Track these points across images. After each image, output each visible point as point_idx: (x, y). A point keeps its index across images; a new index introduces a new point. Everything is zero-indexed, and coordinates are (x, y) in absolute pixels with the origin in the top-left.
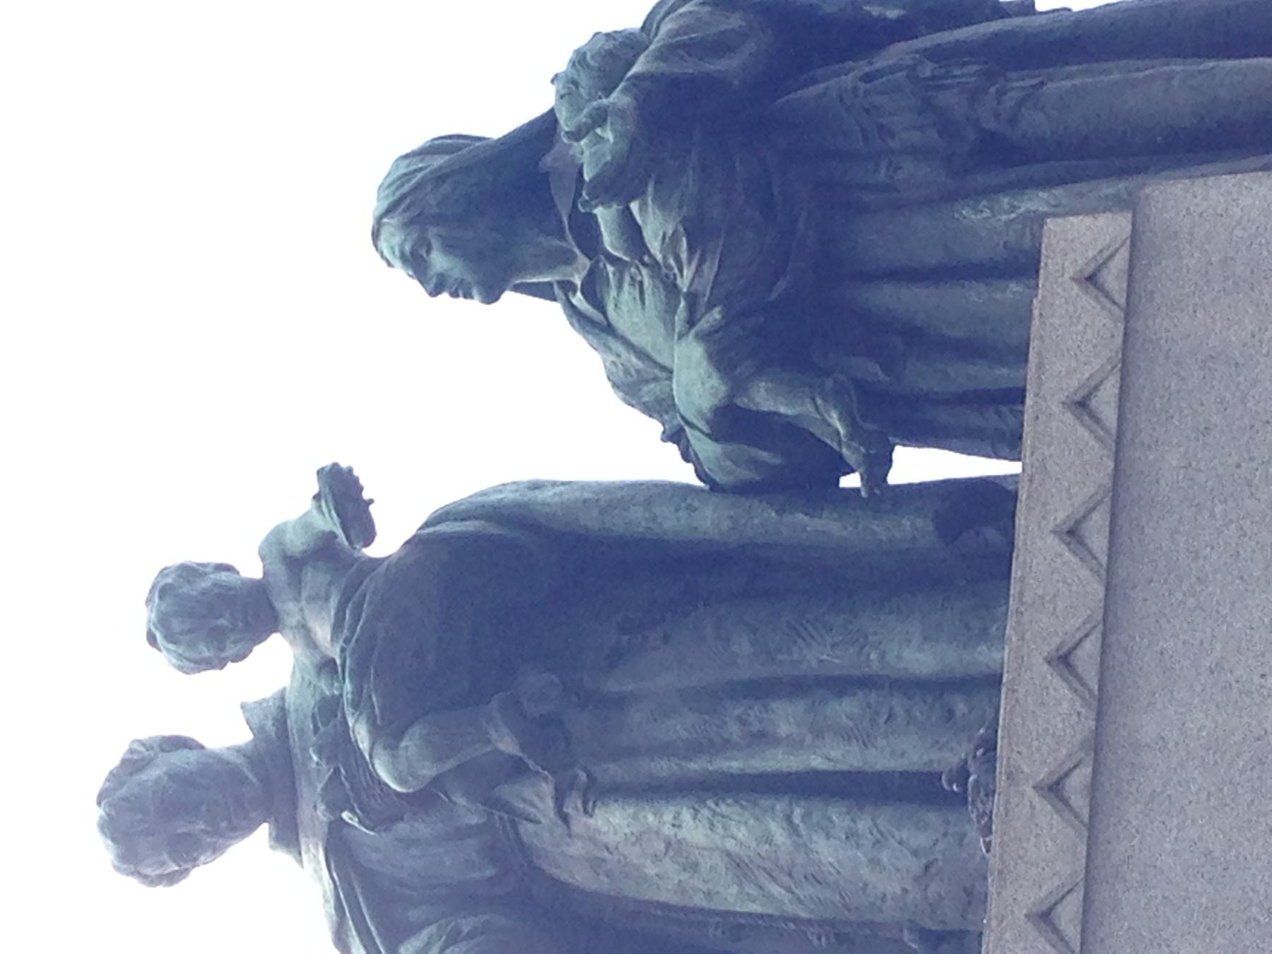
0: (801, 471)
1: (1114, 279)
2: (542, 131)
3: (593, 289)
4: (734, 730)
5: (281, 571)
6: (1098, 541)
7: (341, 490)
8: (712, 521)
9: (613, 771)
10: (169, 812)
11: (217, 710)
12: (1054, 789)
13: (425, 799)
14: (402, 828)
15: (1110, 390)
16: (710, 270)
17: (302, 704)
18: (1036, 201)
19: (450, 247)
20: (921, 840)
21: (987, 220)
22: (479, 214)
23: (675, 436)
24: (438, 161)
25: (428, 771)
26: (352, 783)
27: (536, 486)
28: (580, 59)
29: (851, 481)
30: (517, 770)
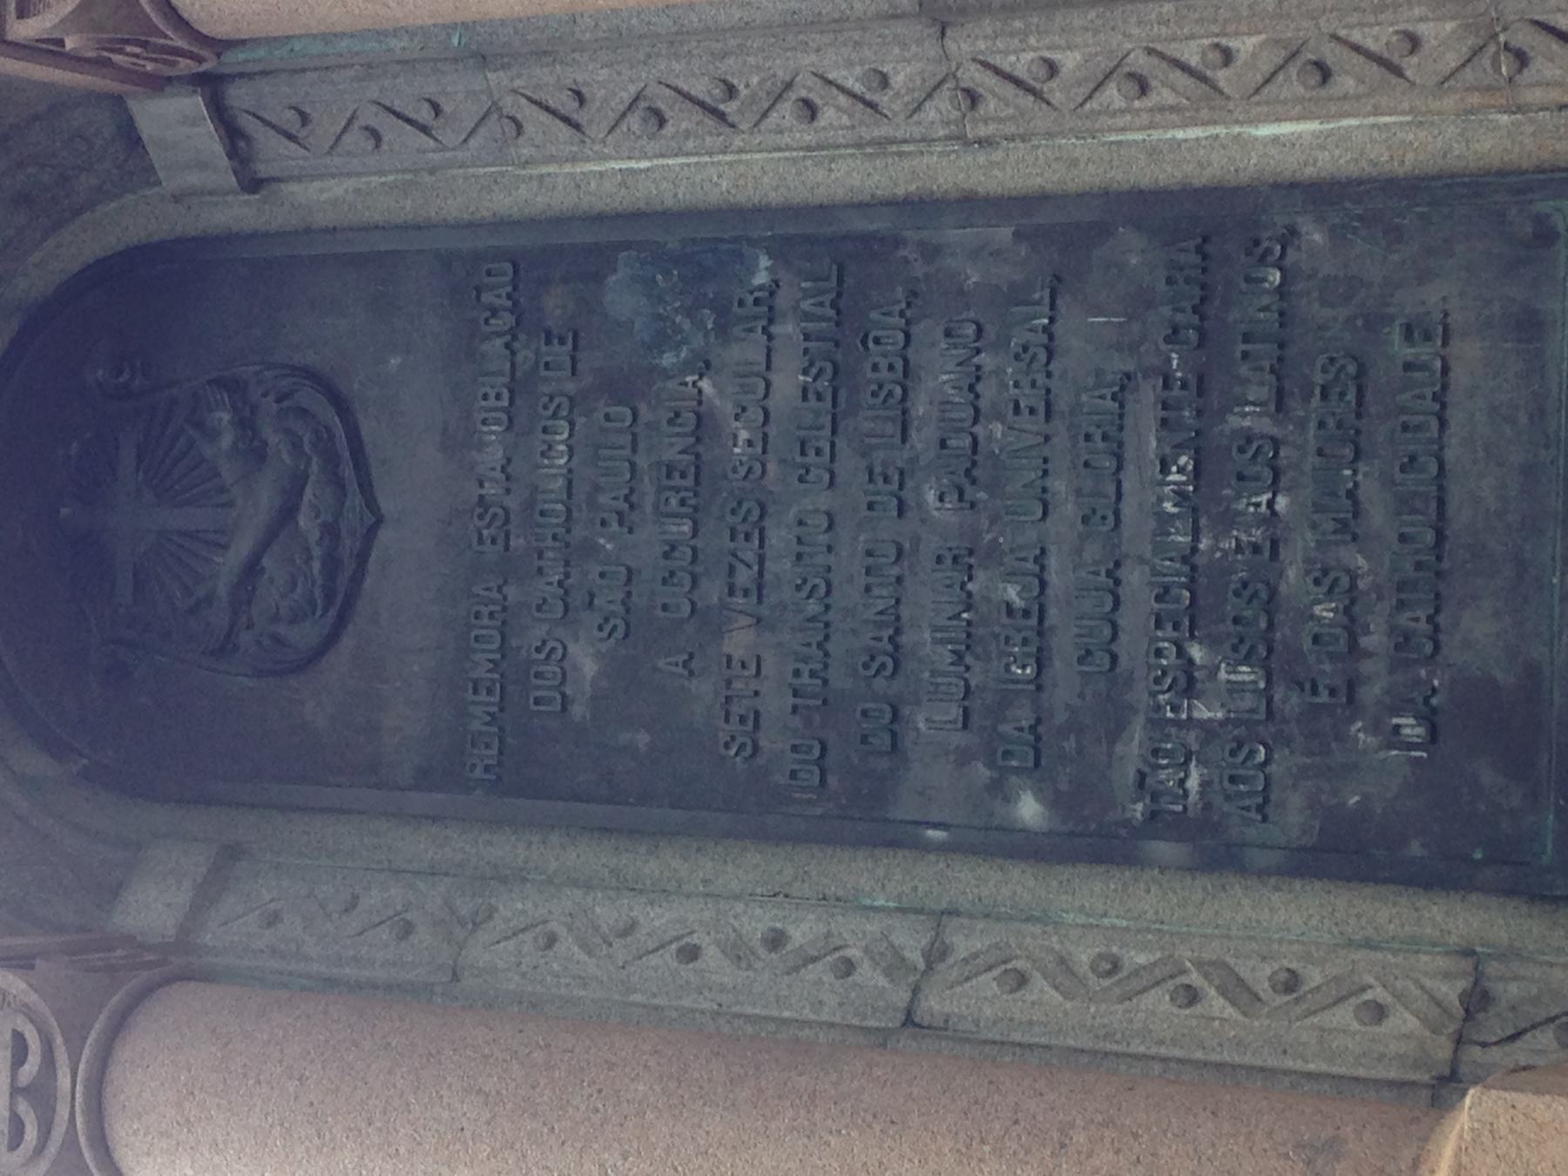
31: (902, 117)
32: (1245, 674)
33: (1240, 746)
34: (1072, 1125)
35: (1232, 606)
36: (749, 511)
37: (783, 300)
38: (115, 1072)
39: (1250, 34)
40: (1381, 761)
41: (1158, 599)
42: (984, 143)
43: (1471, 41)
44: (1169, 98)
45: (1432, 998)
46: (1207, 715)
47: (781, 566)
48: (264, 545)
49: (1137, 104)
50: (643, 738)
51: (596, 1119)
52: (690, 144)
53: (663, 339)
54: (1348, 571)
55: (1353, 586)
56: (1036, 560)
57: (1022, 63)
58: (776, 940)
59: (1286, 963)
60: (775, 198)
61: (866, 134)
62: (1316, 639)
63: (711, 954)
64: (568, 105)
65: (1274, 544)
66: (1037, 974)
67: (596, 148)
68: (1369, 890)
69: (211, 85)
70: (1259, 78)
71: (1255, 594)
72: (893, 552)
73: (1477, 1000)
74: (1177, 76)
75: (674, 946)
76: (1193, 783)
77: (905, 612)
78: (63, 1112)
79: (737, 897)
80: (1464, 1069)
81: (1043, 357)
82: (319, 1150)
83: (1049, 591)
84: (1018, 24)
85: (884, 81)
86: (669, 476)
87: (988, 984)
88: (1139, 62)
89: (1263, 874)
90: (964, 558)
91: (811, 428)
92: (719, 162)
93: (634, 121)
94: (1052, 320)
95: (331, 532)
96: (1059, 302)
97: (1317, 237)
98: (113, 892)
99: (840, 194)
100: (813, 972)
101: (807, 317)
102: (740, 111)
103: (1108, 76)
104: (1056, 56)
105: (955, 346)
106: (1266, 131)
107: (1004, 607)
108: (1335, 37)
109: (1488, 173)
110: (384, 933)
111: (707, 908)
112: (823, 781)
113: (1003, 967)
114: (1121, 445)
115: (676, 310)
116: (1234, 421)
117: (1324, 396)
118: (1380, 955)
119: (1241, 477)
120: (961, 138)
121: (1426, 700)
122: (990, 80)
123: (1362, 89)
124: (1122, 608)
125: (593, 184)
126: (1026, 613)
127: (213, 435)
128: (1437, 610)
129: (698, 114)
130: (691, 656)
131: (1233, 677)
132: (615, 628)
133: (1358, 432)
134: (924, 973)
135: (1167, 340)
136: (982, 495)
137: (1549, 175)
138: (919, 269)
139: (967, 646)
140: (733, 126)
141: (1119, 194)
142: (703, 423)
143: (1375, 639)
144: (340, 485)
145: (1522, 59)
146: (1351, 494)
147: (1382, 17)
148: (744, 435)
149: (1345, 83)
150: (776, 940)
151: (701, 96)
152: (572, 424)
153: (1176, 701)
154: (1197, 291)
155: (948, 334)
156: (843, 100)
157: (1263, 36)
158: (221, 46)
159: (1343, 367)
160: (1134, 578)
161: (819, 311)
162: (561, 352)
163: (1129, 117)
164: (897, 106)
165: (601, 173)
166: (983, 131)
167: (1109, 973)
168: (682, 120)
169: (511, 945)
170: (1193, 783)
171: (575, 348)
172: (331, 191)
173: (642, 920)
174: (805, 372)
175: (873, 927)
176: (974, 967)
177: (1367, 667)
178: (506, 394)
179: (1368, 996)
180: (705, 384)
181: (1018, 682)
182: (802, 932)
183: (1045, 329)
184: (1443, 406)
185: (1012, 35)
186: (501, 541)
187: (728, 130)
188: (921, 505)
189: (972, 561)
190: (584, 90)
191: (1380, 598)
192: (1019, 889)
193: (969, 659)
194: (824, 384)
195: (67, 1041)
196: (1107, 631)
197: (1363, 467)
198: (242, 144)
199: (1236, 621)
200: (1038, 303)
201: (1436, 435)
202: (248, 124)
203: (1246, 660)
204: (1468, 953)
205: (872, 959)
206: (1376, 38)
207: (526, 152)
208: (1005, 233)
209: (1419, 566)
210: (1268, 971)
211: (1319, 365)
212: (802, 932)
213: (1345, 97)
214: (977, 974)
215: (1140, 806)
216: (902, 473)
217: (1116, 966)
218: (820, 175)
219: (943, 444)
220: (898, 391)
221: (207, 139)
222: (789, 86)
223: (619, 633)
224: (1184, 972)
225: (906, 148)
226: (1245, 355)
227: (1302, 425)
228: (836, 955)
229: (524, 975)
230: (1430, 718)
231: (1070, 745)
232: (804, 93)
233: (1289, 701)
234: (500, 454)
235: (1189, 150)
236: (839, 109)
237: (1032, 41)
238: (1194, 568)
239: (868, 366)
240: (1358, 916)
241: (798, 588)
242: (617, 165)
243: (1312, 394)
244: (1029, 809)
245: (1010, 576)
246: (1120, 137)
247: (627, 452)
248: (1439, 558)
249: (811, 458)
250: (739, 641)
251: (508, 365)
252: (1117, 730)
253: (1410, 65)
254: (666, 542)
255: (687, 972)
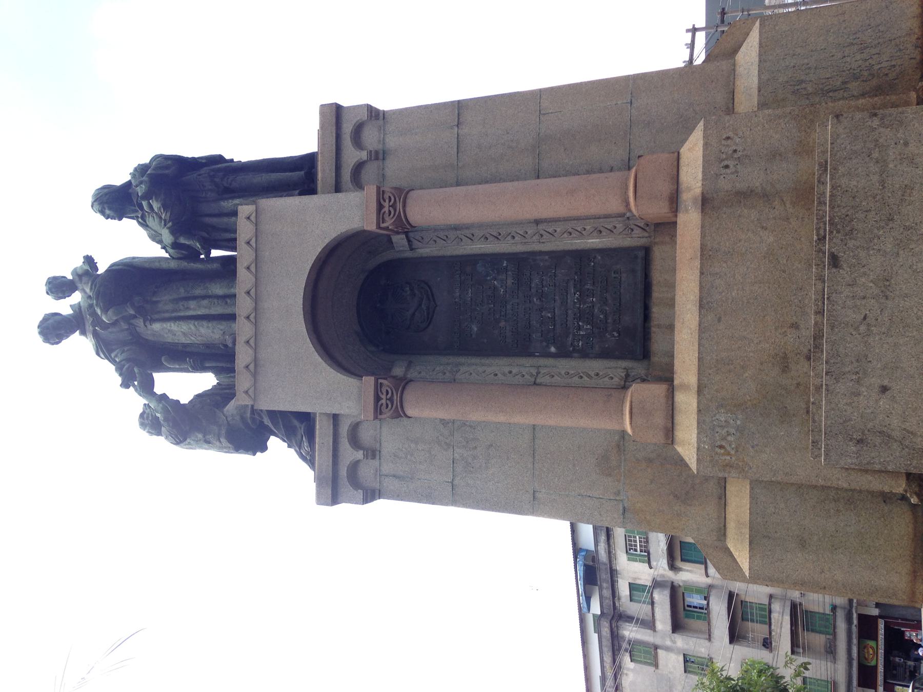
0: (192, 255)
1: (253, 218)
2: (128, 185)
3: (143, 217)
4: (182, 307)
5: (77, 279)
6: (253, 269)
7: (89, 260)
8: (173, 265)
9: (156, 316)
10: (54, 329)
11: (64, 307)
12: (248, 318)
13: (114, 324)
14: (110, 330)
15: (254, 240)
16: (168, 214)
17: (84, 305)
18: (237, 201)
19: (110, 209)
20: (222, 327)
21: (227, 205)
22: (115, 202)
23: (164, 248)
24: (106, 190)
25: (115, 318)
26: (97, 321)
27: (134, 258)
28: (136, 169)
29: (202, 256)
30: (135, 317)
37: (509, 268)
48: (416, 310)
53: (487, 275)
57: (550, 230)
58: (510, 372)
63: (499, 375)
69: (406, 233)
73: (627, 376)
88: (570, 230)
90: (541, 310)
95: (428, 308)
98: (390, 370)
111: (499, 366)
144: (429, 299)
145: (632, 230)
149: (604, 233)
150: (510, 372)
160: (570, 312)
168: (491, 239)
172: (426, 250)
175: (527, 369)
212: (514, 371)
221: (405, 242)
230: (619, 333)
244: (553, 349)
250: (502, 324)
252: (567, 337)
253: (614, 231)
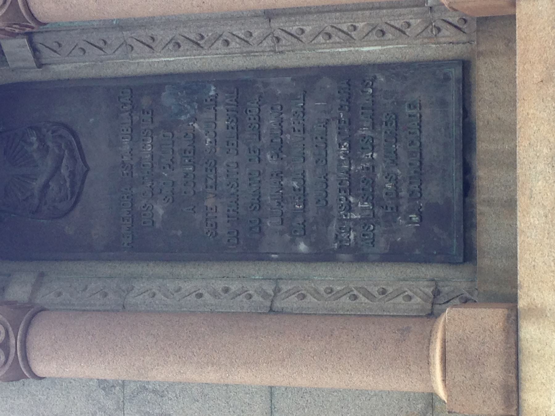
31: (256, 45)
32: (366, 205)
33: (366, 225)
34: (334, 330)
35: (362, 185)
36: (211, 163)
37: (219, 99)
38: (29, 338)
39: (362, 22)
40: (407, 227)
41: (340, 184)
42: (281, 52)
43: (425, 25)
44: (337, 40)
45: (424, 292)
46: (355, 217)
47: (223, 179)
49: (328, 41)
50: (180, 233)
51: (190, 339)
52: (188, 53)
53: (181, 112)
54: (395, 174)
55: (397, 178)
56: (302, 174)
57: (294, 29)
58: (226, 290)
59: (382, 286)
60: (216, 69)
61: (245, 50)
62: (386, 194)
63: (207, 296)
64: (150, 42)
65: (373, 167)
66: (308, 295)
67: (158, 54)
68: (404, 264)
69: (30, 36)
70: (365, 35)
71: (368, 182)
72: (257, 174)
73: (437, 293)
74: (340, 34)
75: (194, 294)
76: (352, 237)
77: (262, 191)
78: (13, 351)
79: (212, 278)
80: (435, 312)
81: (301, 115)
82: (100, 356)
83: (306, 183)
84: (293, 19)
85: (251, 35)
86: (185, 153)
87: (294, 298)
88: (329, 29)
89: (373, 262)
90: (280, 174)
91: (230, 137)
92: (197, 58)
93: (171, 46)
94: (304, 104)
95: (72, 174)
96: (306, 99)
97: (382, 79)
99: (236, 68)
100: (239, 298)
101: (228, 104)
102: (205, 43)
103: (319, 33)
104: (304, 28)
105: (275, 112)
106: (366, 49)
107: (293, 189)
108: (386, 23)
109: (430, 61)
110: (98, 296)
112: (238, 242)
113: (298, 293)
114: (326, 140)
115: (185, 103)
116: (360, 132)
117: (386, 125)
118: (408, 282)
119: (362, 148)
120: (275, 51)
121: (419, 210)
122: (284, 34)
123: (394, 38)
124: (328, 188)
125: (156, 65)
126: (299, 190)
127: (31, 144)
128: (421, 184)
129: (191, 44)
130: (195, 207)
131: (363, 206)
132: (169, 199)
133: (396, 135)
134: (274, 296)
135: (339, 109)
136: (284, 156)
137: (448, 62)
138: (262, 90)
139: (282, 200)
140: (202, 47)
141: (322, 67)
142: (195, 137)
143: (404, 193)
145: (439, 30)
146: (395, 152)
147: (400, 18)
148: (209, 140)
149: (389, 36)
150: (226, 290)
151: (192, 39)
152: (152, 138)
153: (346, 214)
154: (348, 95)
155: (272, 108)
156: (238, 40)
157: (366, 23)
158: (40, 23)
159: (391, 116)
160: (332, 178)
161: (231, 103)
162: (147, 117)
163: (325, 45)
164: (255, 42)
165: (158, 62)
166: (281, 49)
167: (330, 293)
168: (185, 46)
169: (141, 297)
170: (352, 237)
171: (152, 114)
173: (182, 287)
174: (228, 121)
175: (257, 284)
176: (289, 293)
177: (401, 201)
178: (130, 130)
179: (406, 293)
180: (196, 125)
181: (298, 210)
182: (234, 287)
183: (302, 106)
184: (420, 127)
185: (291, 22)
186: (130, 174)
187: (201, 49)
188: (266, 159)
189: (282, 175)
190: (155, 37)
191: (405, 181)
192: (300, 270)
193: (282, 204)
194: (233, 124)
195: (13, 329)
196: (324, 194)
197: (398, 145)
198: (38, 53)
199: (363, 189)
200: (299, 99)
201: (419, 135)
202: (39, 46)
203: (366, 201)
204: (433, 280)
205: (257, 293)
206: (398, 23)
207: (134, 55)
208: (288, 79)
209: (415, 172)
210: (377, 289)
211: (384, 116)
212: (234, 287)
213: (389, 40)
214: (290, 295)
215: (336, 244)
216: (259, 150)
217: (332, 290)
218: (229, 62)
219: (272, 141)
220: (257, 126)
221: (27, 52)
222: (221, 36)
223: (171, 201)
224: (352, 291)
225: (256, 54)
226: (362, 113)
227: (380, 133)
228: (246, 293)
229: (147, 305)
230: (420, 215)
231: (315, 228)
232: (225, 38)
233: (380, 212)
234: (128, 148)
235: (343, 54)
236: (236, 42)
237: (297, 23)
238: (350, 175)
239: (247, 118)
240: (401, 272)
241: (228, 185)
242: (163, 59)
243: (382, 124)
244: (303, 247)
245: (294, 179)
246: (322, 51)
247: (171, 146)
248: (421, 170)
249: (230, 146)
250: (210, 202)
251: (130, 121)
252: (328, 223)
253: (408, 31)
254: (185, 173)
255: (200, 301)
